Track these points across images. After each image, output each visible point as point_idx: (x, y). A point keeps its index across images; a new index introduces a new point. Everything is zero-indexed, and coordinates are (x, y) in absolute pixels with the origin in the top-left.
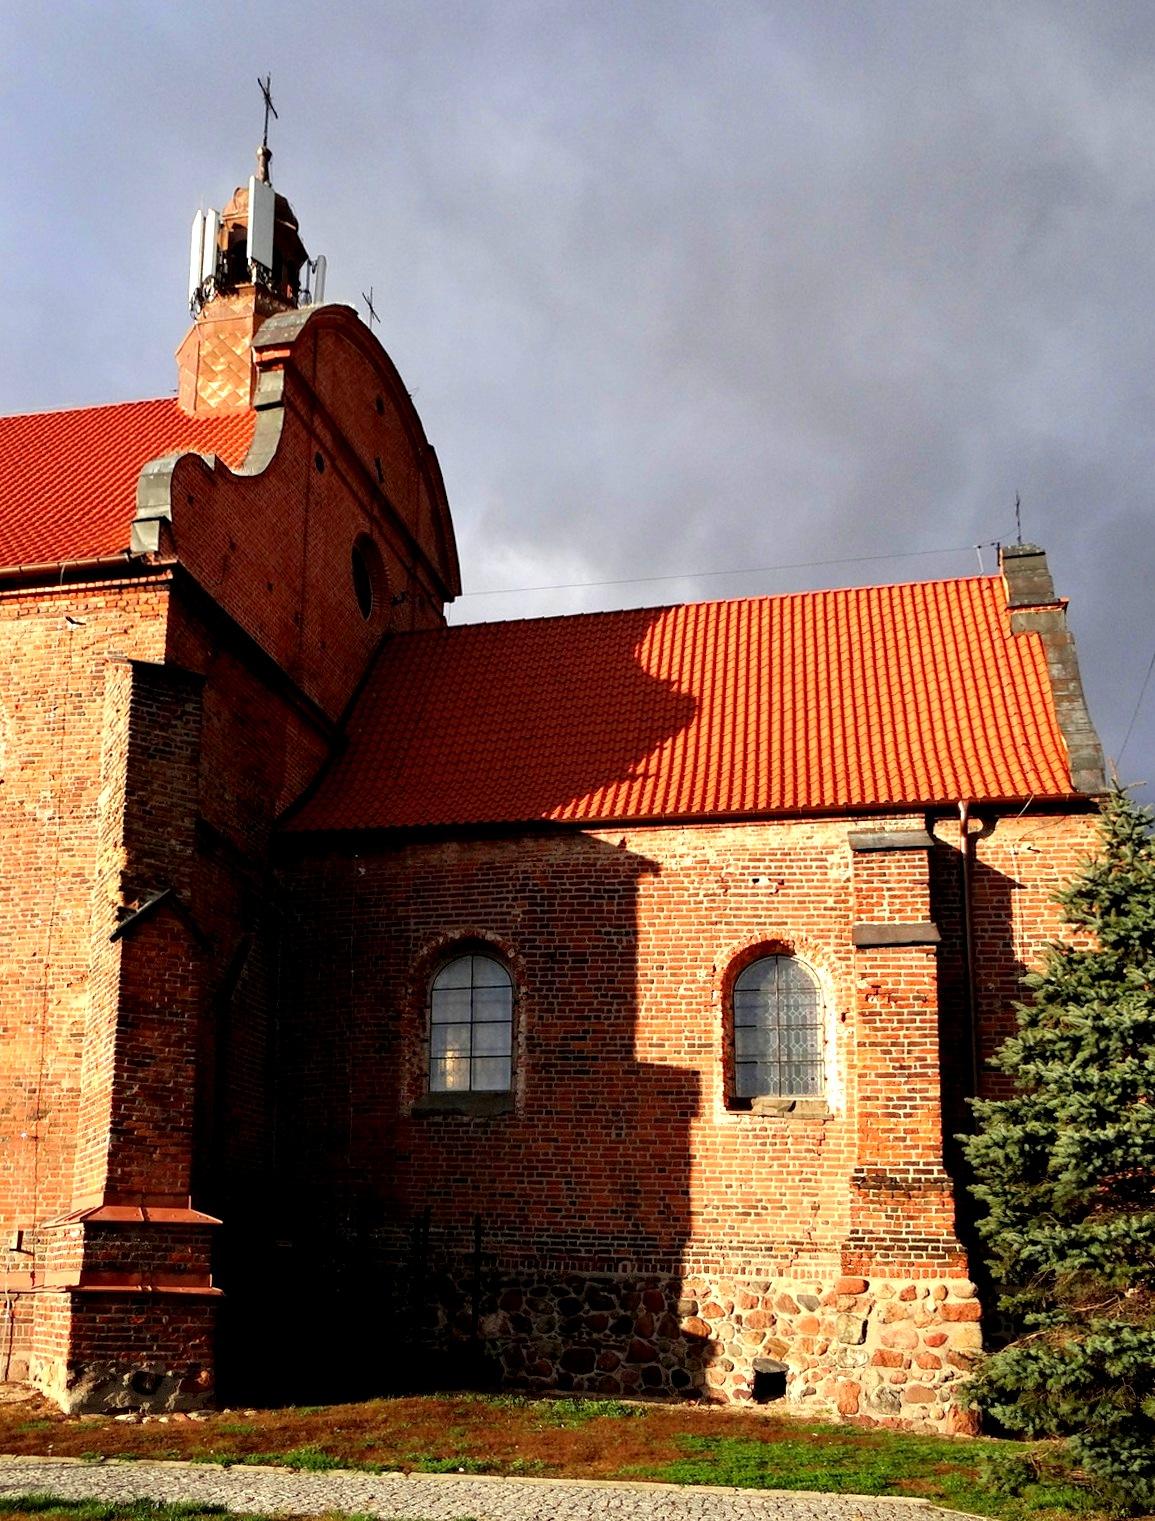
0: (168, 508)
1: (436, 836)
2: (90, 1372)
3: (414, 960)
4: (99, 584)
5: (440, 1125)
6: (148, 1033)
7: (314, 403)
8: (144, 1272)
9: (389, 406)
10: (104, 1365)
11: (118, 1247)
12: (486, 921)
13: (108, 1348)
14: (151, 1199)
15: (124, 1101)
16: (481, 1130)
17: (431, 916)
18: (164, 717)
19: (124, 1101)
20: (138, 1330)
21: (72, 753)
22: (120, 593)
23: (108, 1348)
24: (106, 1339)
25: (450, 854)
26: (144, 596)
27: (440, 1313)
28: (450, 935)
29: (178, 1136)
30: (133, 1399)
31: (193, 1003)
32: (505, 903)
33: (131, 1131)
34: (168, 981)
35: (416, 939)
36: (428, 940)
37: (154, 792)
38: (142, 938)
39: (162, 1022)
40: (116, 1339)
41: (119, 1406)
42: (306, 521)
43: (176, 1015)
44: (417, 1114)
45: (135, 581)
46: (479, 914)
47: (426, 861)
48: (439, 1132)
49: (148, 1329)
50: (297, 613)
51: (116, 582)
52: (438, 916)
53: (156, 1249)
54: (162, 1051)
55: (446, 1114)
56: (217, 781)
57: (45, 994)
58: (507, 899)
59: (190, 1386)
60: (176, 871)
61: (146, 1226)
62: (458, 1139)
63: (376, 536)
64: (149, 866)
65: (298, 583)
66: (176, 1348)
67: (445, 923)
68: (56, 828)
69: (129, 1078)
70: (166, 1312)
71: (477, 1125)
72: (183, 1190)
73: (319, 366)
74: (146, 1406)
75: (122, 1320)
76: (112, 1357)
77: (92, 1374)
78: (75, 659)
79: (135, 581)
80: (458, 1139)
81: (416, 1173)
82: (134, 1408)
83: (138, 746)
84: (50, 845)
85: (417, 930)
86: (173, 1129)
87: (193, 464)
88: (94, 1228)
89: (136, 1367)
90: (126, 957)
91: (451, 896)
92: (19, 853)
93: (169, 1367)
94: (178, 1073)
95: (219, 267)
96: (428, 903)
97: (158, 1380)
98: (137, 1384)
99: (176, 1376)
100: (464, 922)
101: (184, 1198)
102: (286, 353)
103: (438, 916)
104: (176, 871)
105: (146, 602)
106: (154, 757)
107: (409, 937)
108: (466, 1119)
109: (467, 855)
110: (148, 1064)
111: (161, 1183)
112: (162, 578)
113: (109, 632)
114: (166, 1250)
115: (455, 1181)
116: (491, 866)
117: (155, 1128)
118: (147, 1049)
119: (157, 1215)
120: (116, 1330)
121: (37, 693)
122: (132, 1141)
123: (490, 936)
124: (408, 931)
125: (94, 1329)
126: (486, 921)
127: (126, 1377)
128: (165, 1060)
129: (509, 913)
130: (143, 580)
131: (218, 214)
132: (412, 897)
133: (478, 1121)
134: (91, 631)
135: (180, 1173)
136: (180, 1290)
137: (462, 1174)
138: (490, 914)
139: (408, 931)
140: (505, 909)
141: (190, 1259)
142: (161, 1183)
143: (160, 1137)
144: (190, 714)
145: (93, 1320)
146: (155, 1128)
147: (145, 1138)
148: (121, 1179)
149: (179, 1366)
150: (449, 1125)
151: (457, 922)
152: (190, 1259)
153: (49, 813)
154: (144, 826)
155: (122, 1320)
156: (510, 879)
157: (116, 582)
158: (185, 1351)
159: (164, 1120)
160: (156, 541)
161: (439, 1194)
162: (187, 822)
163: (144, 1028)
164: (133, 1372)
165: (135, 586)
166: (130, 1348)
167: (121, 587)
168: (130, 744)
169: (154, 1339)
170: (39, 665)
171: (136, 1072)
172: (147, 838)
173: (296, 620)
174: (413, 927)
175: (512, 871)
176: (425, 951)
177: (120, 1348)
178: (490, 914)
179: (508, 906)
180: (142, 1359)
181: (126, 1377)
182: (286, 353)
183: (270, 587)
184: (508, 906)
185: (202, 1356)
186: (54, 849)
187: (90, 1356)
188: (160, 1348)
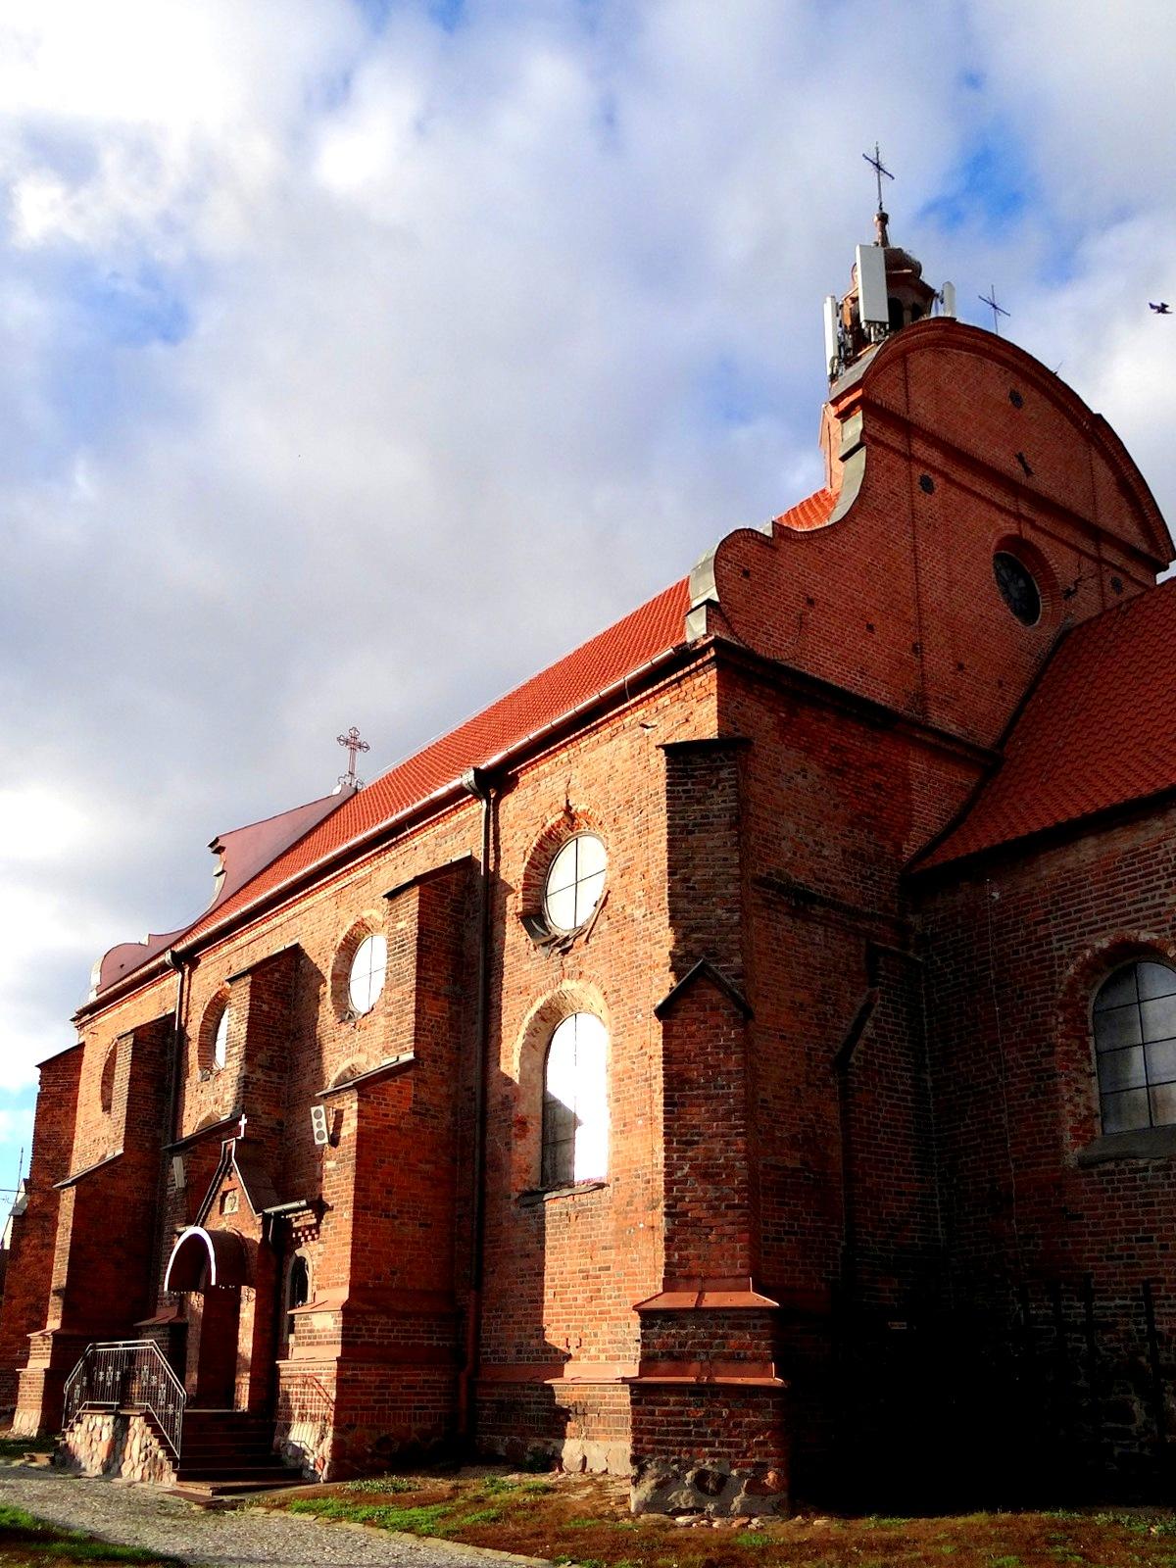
0: (714, 590)
1: (1066, 834)
2: (652, 1469)
3: (1061, 983)
4: (662, 684)
5: (1112, 1173)
6: (695, 1110)
7: (908, 428)
8: (702, 1362)
9: (1028, 394)
10: (666, 1461)
11: (673, 1336)
12: (1138, 920)
13: (670, 1443)
14: (711, 1283)
15: (675, 1183)
16: (1160, 1174)
17: (1073, 929)
18: (700, 791)
19: (675, 1183)
20: (698, 1424)
21: (655, 850)
22: (680, 686)
23: (670, 1443)
24: (667, 1433)
25: (1087, 851)
26: (697, 681)
27: (1136, 1407)
28: (1098, 945)
29: (731, 1215)
30: (696, 1500)
31: (738, 1072)
32: (1158, 892)
33: (685, 1214)
34: (711, 1054)
35: (1062, 957)
36: (1074, 956)
37: (695, 867)
38: (681, 1014)
39: (708, 1098)
40: (676, 1433)
41: (684, 1507)
42: (915, 549)
43: (723, 1087)
44: (1085, 1164)
45: (687, 669)
46: (1129, 913)
47: (1061, 867)
48: (1111, 1182)
49: (709, 1424)
50: (914, 645)
51: (674, 677)
52: (1082, 927)
53: (714, 1336)
54: (710, 1127)
55: (1117, 1159)
56: (810, 839)
57: (650, 1085)
58: (1158, 887)
59: (755, 1487)
60: (723, 941)
61: (698, 1312)
62: (1135, 1188)
63: (1029, 534)
64: (698, 941)
65: (912, 614)
66: (738, 1445)
67: (1091, 932)
68: (648, 924)
69: (679, 1158)
70: (726, 1405)
71: (1157, 1169)
72: (743, 1271)
73: (912, 390)
74: (711, 1507)
75: (681, 1413)
76: (673, 1453)
77: (655, 1471)
78: (652, 761)
79: (687, 669)
80: (1135, 1188)
81: (1091, 1234)
82: (697, 1510)
83: (677, 826)
84: (645, 942)
85: (1061, 948)
86: (728, 1207)
87: (745, 539)
88: (649, 1317)
89: (699, 1465)
90: (667, 1035)
91: (1095, 899)
92: (624, 955)
93: (733, 1466)
94: (727, 1149)
95: (841, 345)
96: (1069, 914)
97: (722, 1481)
98: (701, 1478)
99: (741, 1475)
100: (1112, 926)
101: (745, 1280)
102: (859, 393)
103: (1082, 927)
104: (723, 941)
105: (700, 686)
106: (693, 832)
107: (1053, 958)
108: (1142, 1163)
109: (1105, 848)
110: (697, 1143)
111: (719, 1266)
112: (708, 657)
113: (675, 725)
114: (724, 1337)
115: (1138, 1240)
116: (1134, 852)
117: (708, 1209)
118: (694, 1127)
119: (712, 1300)
120: (676, 1424)
121: (627, 802)
122: (686, 1224)
123: (1144, 936)
124: (1051, 950)
125: (654, 1423)
126: (1138, 920)
127: (689, 1475)
128: (714, 1136)
129: (1163, 904)
130: (693, 666)
131: (833, 297)
132: (1050, 912)
133: (1158, 1163)
134: (661, 730)
135: (738, 1253)
136: (739, 1381)
137: (1145, 1231)
138: (1141, 910)
139: (1051, 950)
140: (1158, 901)
141: (749, 1347)
142: (719, 1266)
143: (715, 1216)
144: (727, 780)
145: (652, 1413)
146: (708, 1209)
147: (700, 1219)
148: (679, 1265)
149: (744, 1465)
150: (1122, 1172)
151: (1104, 928)
152: (749, 1347)
153: (643, 911)
154: (689, 902)
155: (681, 1413)
156: (1160, 863)
157: (674, 677)
158: (749, 1448)
159: (717, 1199)
160: (704, 624)
161: (1120, 1258)
162: (732, 889)
163: (692, 1105)
164: (695, 1470)
165: (688, 674)
166: (690, 1444)
167: (678, 680)
168: (669, 826)
169: (716, 1434)
170: (628, 776)
171: (685, 1151)
172: (693, 914)
173: (915, 649)
174: (1056, 945)
175: (1160, 853)
176: (1071, 970)
177: (681, 1444)
178: (1141, 910)
179: (1161, 896)
180: (705, 1456)
181: (689, 1475)
182: (859, 393)
183: (870, 628)
184: (1161, 896)
185: (767, 1455)
186: (648, 944)
187: (652, 1451)
188: (722, 1444)
